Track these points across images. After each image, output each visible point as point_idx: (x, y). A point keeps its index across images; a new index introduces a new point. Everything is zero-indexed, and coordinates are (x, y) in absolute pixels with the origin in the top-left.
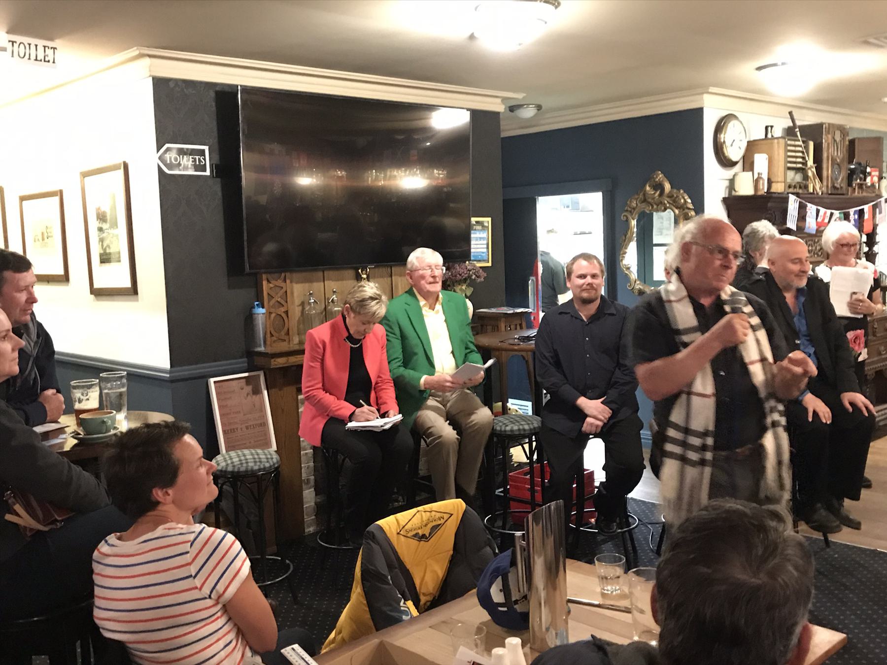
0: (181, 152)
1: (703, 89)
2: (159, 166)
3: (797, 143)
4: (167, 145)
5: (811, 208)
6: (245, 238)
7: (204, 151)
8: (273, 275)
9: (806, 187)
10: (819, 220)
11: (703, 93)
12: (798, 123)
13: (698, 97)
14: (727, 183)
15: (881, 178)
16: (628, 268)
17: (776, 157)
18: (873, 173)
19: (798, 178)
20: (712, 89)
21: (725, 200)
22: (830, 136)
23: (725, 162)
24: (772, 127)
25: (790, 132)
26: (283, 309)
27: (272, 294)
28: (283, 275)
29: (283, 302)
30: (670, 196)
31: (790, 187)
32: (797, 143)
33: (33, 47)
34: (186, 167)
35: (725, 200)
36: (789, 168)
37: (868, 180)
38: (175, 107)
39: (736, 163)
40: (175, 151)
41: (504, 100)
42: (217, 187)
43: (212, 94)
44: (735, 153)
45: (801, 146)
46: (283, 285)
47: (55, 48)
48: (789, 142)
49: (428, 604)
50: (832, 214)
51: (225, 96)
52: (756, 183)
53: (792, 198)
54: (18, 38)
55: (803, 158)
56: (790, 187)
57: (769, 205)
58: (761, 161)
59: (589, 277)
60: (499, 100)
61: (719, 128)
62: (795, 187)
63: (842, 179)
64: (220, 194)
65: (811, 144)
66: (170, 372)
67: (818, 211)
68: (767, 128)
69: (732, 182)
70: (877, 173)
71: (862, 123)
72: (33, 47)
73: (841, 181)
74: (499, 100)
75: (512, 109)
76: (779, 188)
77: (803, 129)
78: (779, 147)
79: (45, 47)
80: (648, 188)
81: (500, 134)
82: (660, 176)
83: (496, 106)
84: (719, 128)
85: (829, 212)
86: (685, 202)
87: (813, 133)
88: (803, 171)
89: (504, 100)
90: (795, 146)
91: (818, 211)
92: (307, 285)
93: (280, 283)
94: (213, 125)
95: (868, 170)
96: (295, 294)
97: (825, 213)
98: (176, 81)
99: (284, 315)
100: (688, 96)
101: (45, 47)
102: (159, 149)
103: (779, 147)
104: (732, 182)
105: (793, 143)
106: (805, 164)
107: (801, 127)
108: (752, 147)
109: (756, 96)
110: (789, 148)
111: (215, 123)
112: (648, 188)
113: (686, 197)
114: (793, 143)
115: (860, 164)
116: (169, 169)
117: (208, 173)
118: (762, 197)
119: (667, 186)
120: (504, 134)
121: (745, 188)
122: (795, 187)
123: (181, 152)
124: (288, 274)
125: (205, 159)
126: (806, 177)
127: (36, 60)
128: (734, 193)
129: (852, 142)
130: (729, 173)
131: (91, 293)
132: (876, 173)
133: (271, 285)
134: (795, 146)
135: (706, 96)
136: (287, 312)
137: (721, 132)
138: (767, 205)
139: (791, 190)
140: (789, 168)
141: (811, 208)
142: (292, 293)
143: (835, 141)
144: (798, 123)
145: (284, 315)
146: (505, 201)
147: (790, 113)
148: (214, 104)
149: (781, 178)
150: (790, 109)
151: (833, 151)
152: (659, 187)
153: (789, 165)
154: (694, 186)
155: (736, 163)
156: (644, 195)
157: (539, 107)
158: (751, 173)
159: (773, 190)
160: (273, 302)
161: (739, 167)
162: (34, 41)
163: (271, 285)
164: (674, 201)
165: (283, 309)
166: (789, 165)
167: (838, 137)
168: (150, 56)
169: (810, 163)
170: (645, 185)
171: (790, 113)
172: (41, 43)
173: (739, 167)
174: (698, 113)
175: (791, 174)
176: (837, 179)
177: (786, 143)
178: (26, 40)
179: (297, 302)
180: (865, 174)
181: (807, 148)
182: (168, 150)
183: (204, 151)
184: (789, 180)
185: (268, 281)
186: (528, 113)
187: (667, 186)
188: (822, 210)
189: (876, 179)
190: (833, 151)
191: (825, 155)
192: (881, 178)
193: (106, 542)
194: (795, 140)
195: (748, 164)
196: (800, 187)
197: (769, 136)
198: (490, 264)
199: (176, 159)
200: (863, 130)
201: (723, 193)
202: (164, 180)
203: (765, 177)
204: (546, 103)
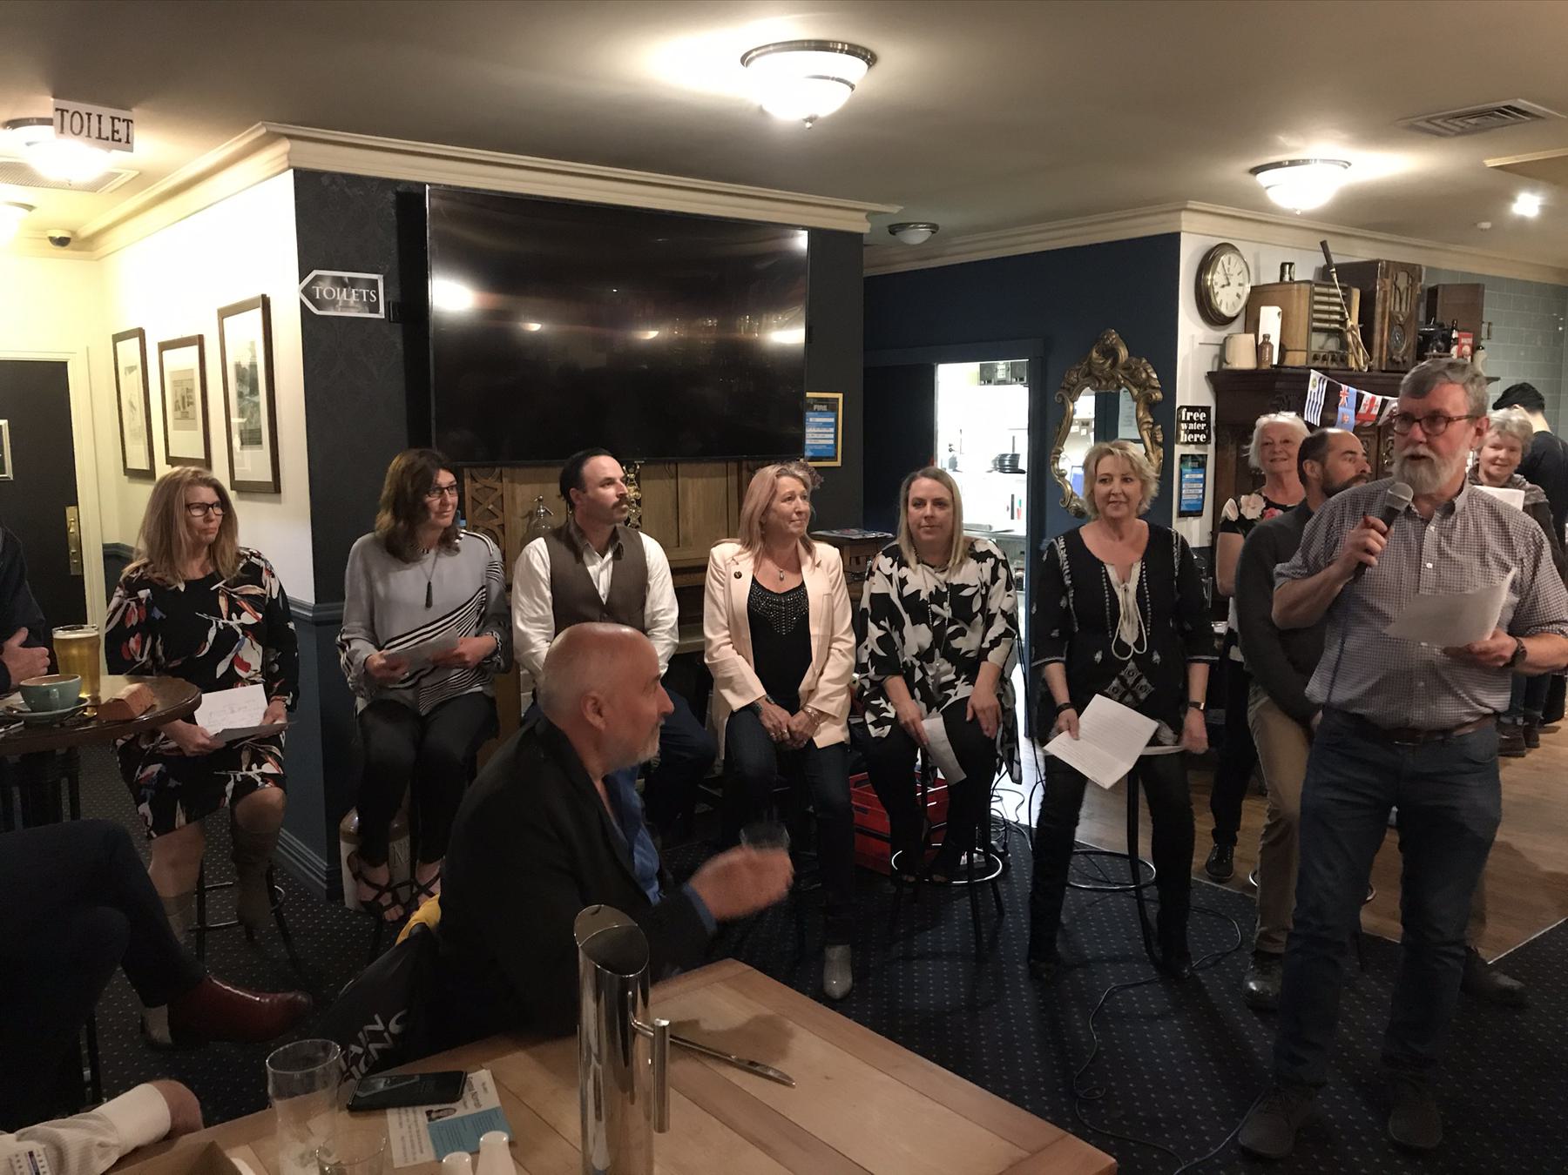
0: (339, 282)
1: (1178, 204)
2: (302, 302)
3: (1332, 291)
4: (315, 273)
5: (1348, 392)
6: (433, 414)
7: (375, 282)
9: (1344, 359)
10: (1362, 410)
12: (1336, 260)
13: (1172, 216)
14: (1216, 350)
15: (1476, 348)
16: (1063, 476)
17: (1295, 312)
18: (1463, 341)
19: (1332, 345)
20: (1192, 204)
21: (1211, 376)
22: (1388, 281)
23: (1209, 313)
24: (1291, 264)
25: (1324, 274)
26: (496, 522)
27: (480, 499)
28: (498, 470)
29: (497, 512)
30: (1127, 368)
31: (1315, 358)
32: (1332, 291)
33: (94, 119)
34: (348, 305)
35: (1211, 376)
36: (1316, 330)
37: (1454, 350)
38: (333, 219)
39: (1233, 319)
40: (328, 282)
41: (871, 215)
42: (396, 337)
43: (391, 197)
44: (1228, 300)
45: (1337, 296)
46: (497, 485)
47: (129, 121)
48: (1317, 289)
50: (1384, 403)
51: (409, 198)
52: (1259, 349)
53: (1314, 375)
54: (64, 104)
55: (1342, 314)
56: (1315, 358)
57: (1278, 385)
58: (1270, 320)
59: (1117, 481)
60: (863, 215)
61: (1207, 263)
62: (1324, 359)
63: (1408, 348)
64: (400, 347)
65: (1356, 295)
66: (314, 610)
67: (1360, 398)
68: (1283, 265)
69: (1223, 347)
70: (1470, 341)
71: (1450, 262)
72: (94, 119)
73: (1404, 348)
74: (863, 215)
75: (894, 229)
76: (1297, 359)
77: (1341, 269)
78: (1299, 296)
79: (113, 118)
80: (1095, 354)
82: (1113, 337)
83: (855, 222)
84: (1207, 263)
85: (1379, 399)
86: (1149, 376)
87: (1360, 276)
88: (1339, 334)
89: (871, 215)
90: (1329, 295)
91: (1360, 398)
92: (538, 486)
93: (491, 482)
94: (393, 243)
95: (1455, 335)
96: (519, 500)
97: (1373, 400)
98: (334, 177)
99: (497, 530)
100: (1156, 214)
101: (113, 118)
103: (1299, 296)
104: (1223, 347)
105: (1325, 290)
106: (1343, 323)
107: (1340, 267)
108: (1259, 296)
109: (1259, 213)
110: (1317, 298)
111: (394, 240)
112: (1095, 354)
114: (1325, 290)
115: (1442, 325)
117: (381, 315)
118: (1267, 372)
119: (1123, 353)
120: (868, 272)
121: (1242, 358)
122: (1324, 359)
123: (339, 282)
124: (506, 470)
125: (377, 295)
126: (1344, 345)
127: (100, 137)
128: (1225, 366)
129: (1433, 293)
130: (1218, 335)
132: (1467, 342)
133: (478, 486)
134: (1329, 295)
135: (1184, 215)
136: (502, 527)
137: (1207, 273)
138: (1274, 385)
139: (1318, 364)
140: (1316, 330)
141: (1348, 392)
142: (513, 498)
143: (1397, 288)
144: (1336, 260)
145: (497, 530)
146: (865, 370)
147: (1323, 244)
148: (393, 212)
149: (1302, 345)
150: (1322, 238)
151: (1393, 302)
152: (1111, 353)
153: (1316, 324)
155: (1233, 319)
156: (1089, 364)
157: (934, 228)
158: (1252, 336)
159: (1288, 362)
161: (1238, 325)
162: (96, 110)
163: (478, 486)
164: (1132, 375)
165: (496, 522)
166: (1316, 324)
167: (1402, 282)
168: (290, 137)
169: (1353, 322)
170: (1090, 351)
171: (1323, 244)
172: (107, 112)
173: (1238, 325)
174: (1171, 242)
175: (1318, 340)
176: (1397, 348)
177: (1312, 289)
178: (84, 108)
179: (520, 511)
180: (1448, 343)
181: (1347, 298)
182: (317, 278)
183: (375, 282)
184: (1315, 348)
185: (473, 479)
186: (918, 236)
187: (1123, 353)
188: (1368, 396)
189: (1467, 349)
190: (1393, 302)
191: (1379, 309)
192: (1476, 348)
194: (1329, 286)
195: (1251, 321)
196: (1333, 360)
197: (1287, 278)
198: (838, 463)
199: (330, 293)
200: (1453, 273)
201: (1209, 366)
202: (311, 325)
203: (1275, 341)
204: (946, 220)
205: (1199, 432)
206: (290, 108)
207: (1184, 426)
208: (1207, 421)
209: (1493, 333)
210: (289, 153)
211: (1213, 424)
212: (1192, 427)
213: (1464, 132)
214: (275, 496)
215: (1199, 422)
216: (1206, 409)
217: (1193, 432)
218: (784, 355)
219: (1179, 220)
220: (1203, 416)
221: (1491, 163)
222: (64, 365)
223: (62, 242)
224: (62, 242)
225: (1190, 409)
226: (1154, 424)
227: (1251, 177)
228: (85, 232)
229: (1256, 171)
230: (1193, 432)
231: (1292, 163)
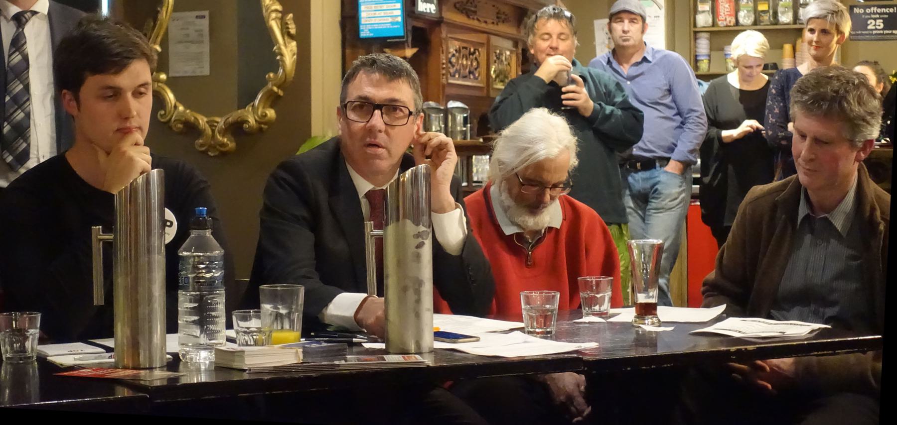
193: (714, 24)
226: (284, 13)
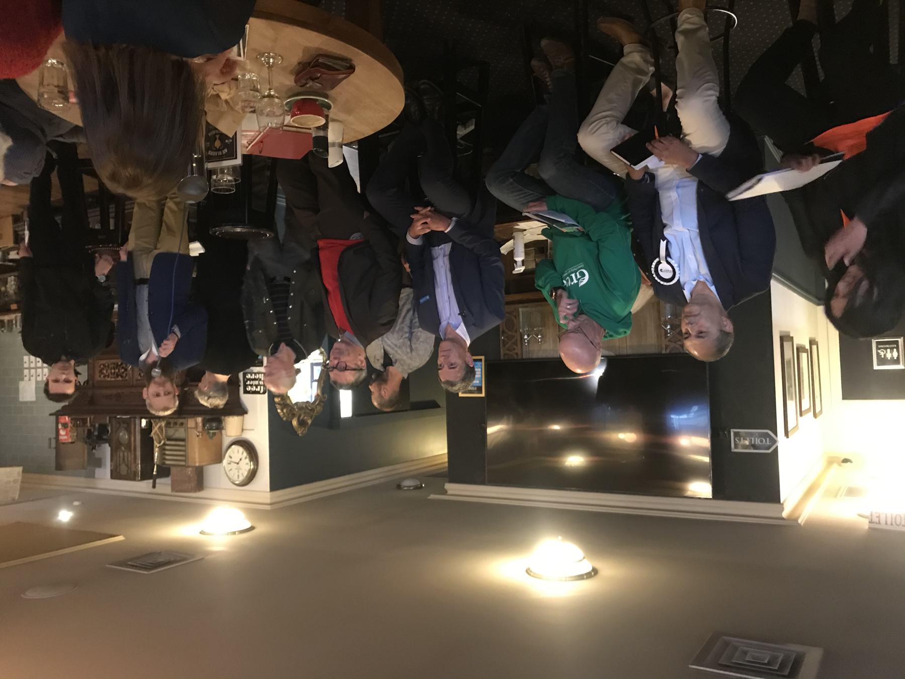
2: (776, 434)
8: (677, 351)
11: (271, 504)
13: (273, 501)
20: (268, 508)
28: (668, 351)
30: (294, 415)
36: (183, 440)
41: (445, 492)
48: (183, 463)
49: (633, 66)
74: (449, 492)
81: (172, 481)
102: (776, 450)
113: (281, 414)
116: (768, 434)
119: (295, 423)
122: (176, 424)
131: (792, 338)
135: (268, 501)
140: (183, 440)
143: (127, 466)
152: (302, 423)
154: (278, 427)
160: (513, 340)
182: (768, 448)
187: (295, 423)
205: (250, 380)
206: (785, 532)
207: (261, 383)
208: (245, 386)
209: (47, 441)
210: (783, 510)
211: (242, 384)
212: (257, 382)
213: (151, 554)
214: (783, 334)
215: (251, 385)
216: (246, 392)
217: (255, 379)
218: (498, 418)
219: (271, 499)
220: (249, 389)
221: (121, 538)
222: (844, 398)
223: (846, 461)
224: (846, 461)
225: (258, 393)
227: (254, 525)
228: (835, 466)
229: (252, 528)
230: (255, 379)
231: (234, 533)
